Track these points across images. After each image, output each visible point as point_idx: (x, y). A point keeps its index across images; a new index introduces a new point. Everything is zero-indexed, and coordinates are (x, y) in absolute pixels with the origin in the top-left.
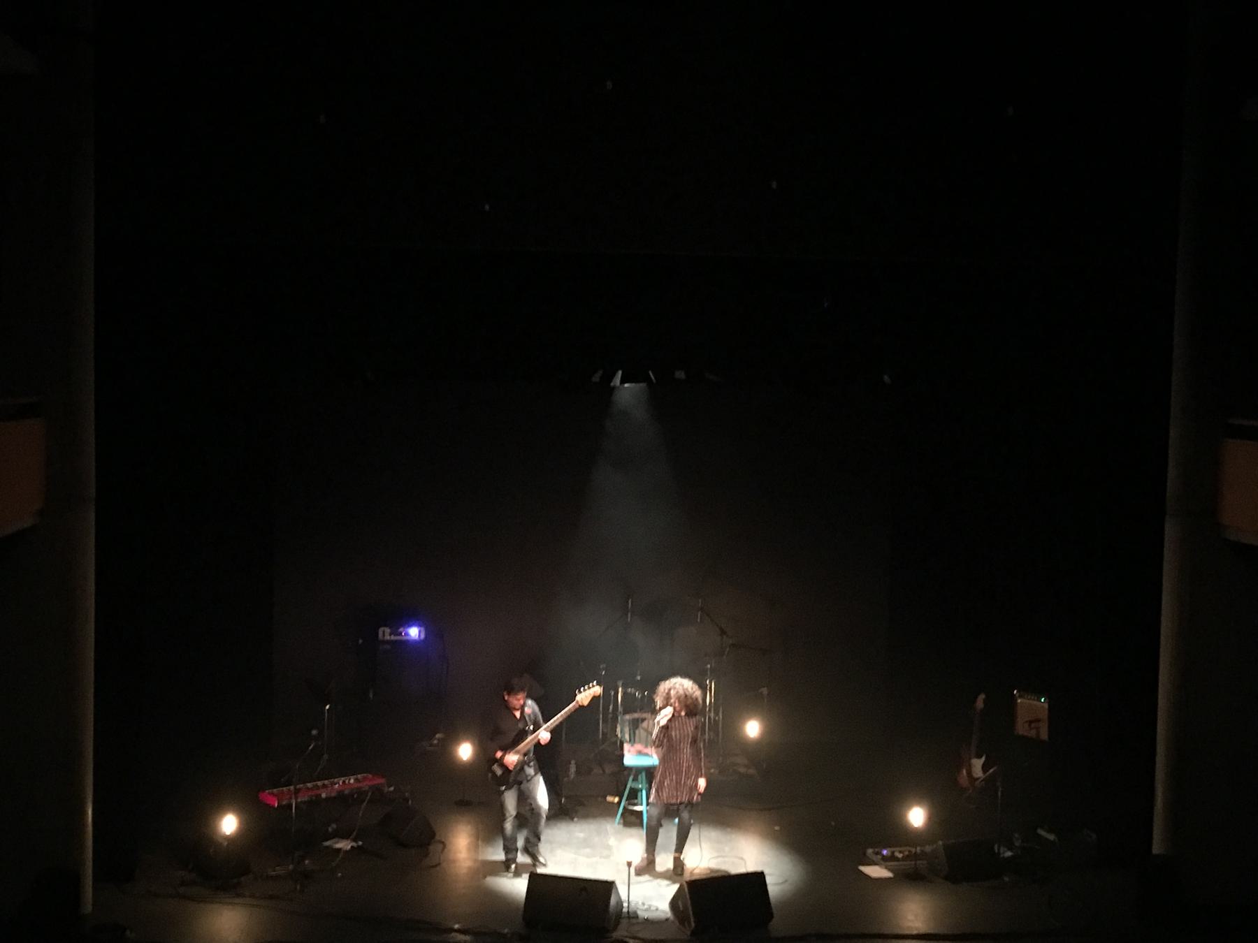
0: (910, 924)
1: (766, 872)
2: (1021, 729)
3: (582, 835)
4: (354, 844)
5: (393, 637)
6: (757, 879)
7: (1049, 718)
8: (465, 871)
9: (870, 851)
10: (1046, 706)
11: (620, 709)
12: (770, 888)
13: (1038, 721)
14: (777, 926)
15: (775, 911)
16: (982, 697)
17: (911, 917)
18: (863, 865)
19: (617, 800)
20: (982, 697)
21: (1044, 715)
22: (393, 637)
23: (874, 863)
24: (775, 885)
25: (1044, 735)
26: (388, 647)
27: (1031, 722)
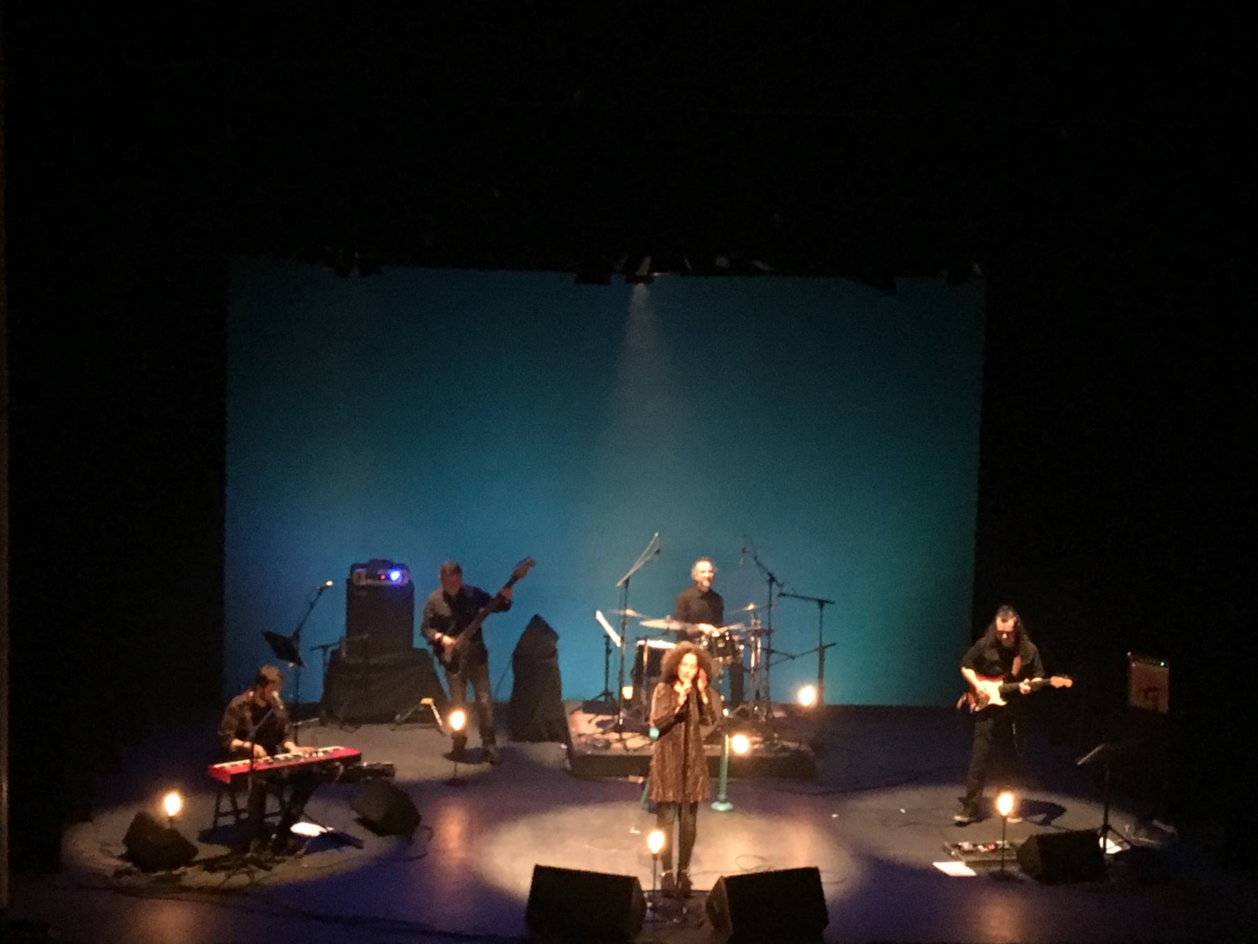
0: (994, 933)
1: (821, 868)
2: (1135, 700)
3: (599, 822)
4: (324, 830)
5: (370, 581)
6: (810, 876)
7: (1170, 689)
8: (454, 863)
9: (220, 733)
10: (1167, 670)
11: (645, 671)
12: (825, 888)
13: (1154, 689)
14: (828, 933)
15: (829, 909)
16: (1068, 683)
17: (995, 923)
18: (972, 877)
19: (641, 780)
20: (1068, 683)
21: (1164, 682)
22: (370, 581)
23: (956, 859)
24: (831, 886)
25: (1163, 706)
26: (364, 594)
27: (1147, 691)
